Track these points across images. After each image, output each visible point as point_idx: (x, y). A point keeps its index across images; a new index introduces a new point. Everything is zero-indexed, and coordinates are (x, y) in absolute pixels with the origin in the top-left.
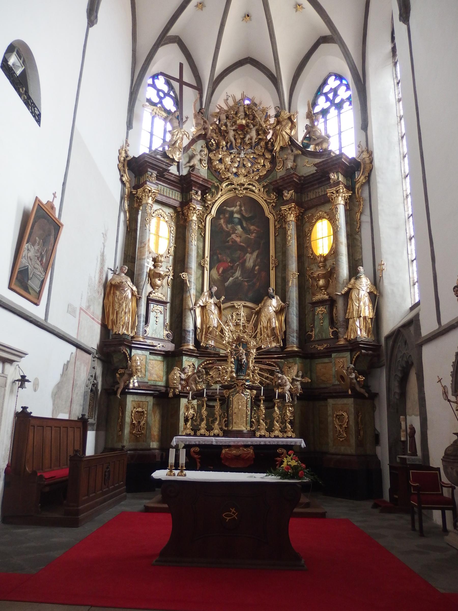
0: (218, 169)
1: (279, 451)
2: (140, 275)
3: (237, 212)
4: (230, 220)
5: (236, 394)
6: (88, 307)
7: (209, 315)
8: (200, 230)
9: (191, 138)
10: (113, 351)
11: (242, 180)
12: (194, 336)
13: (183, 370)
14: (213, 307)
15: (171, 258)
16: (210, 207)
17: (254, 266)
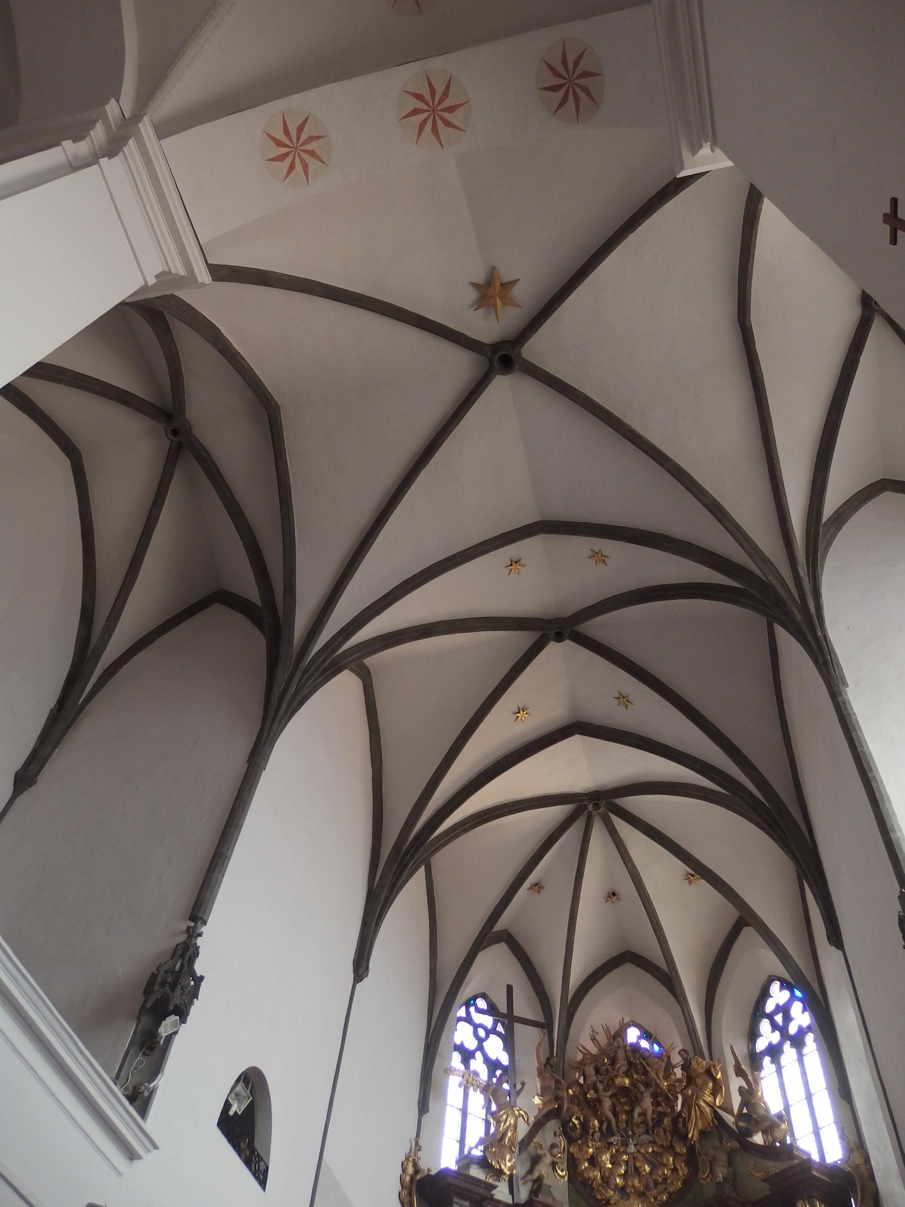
0: (589, 1178)
9: (532, 1120)
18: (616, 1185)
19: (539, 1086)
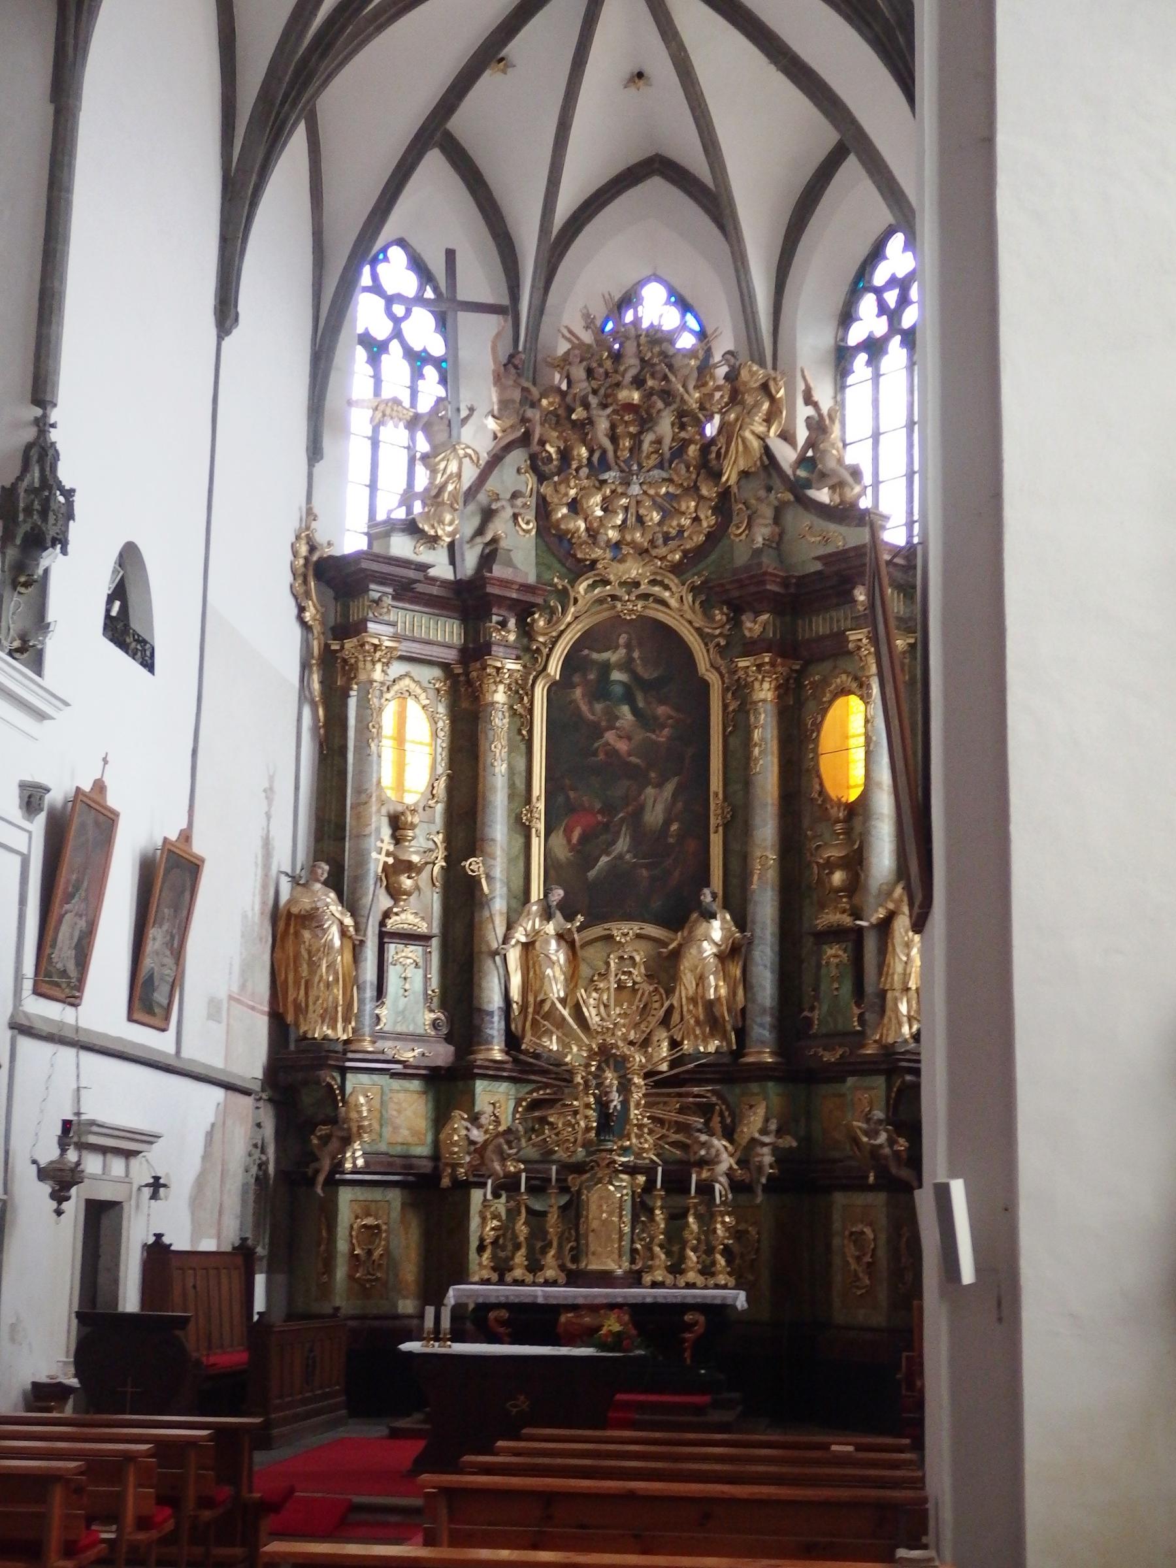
0: (568, 531)
1: (688, 1317)
2: (359, 879)
4: (601, 690)
5: (596, 1184)
6: (243, 987)
7: (543, 968)
8: (517, 719)
10: (300, 1083)
11: (633, 569)
12: (503, 1023)
13: (475, 1119)
14: (553, 944)
15: (440, 808)
16: (545, 651)
17: (667, 823)
18: (609, 540)
19: (495, 399)
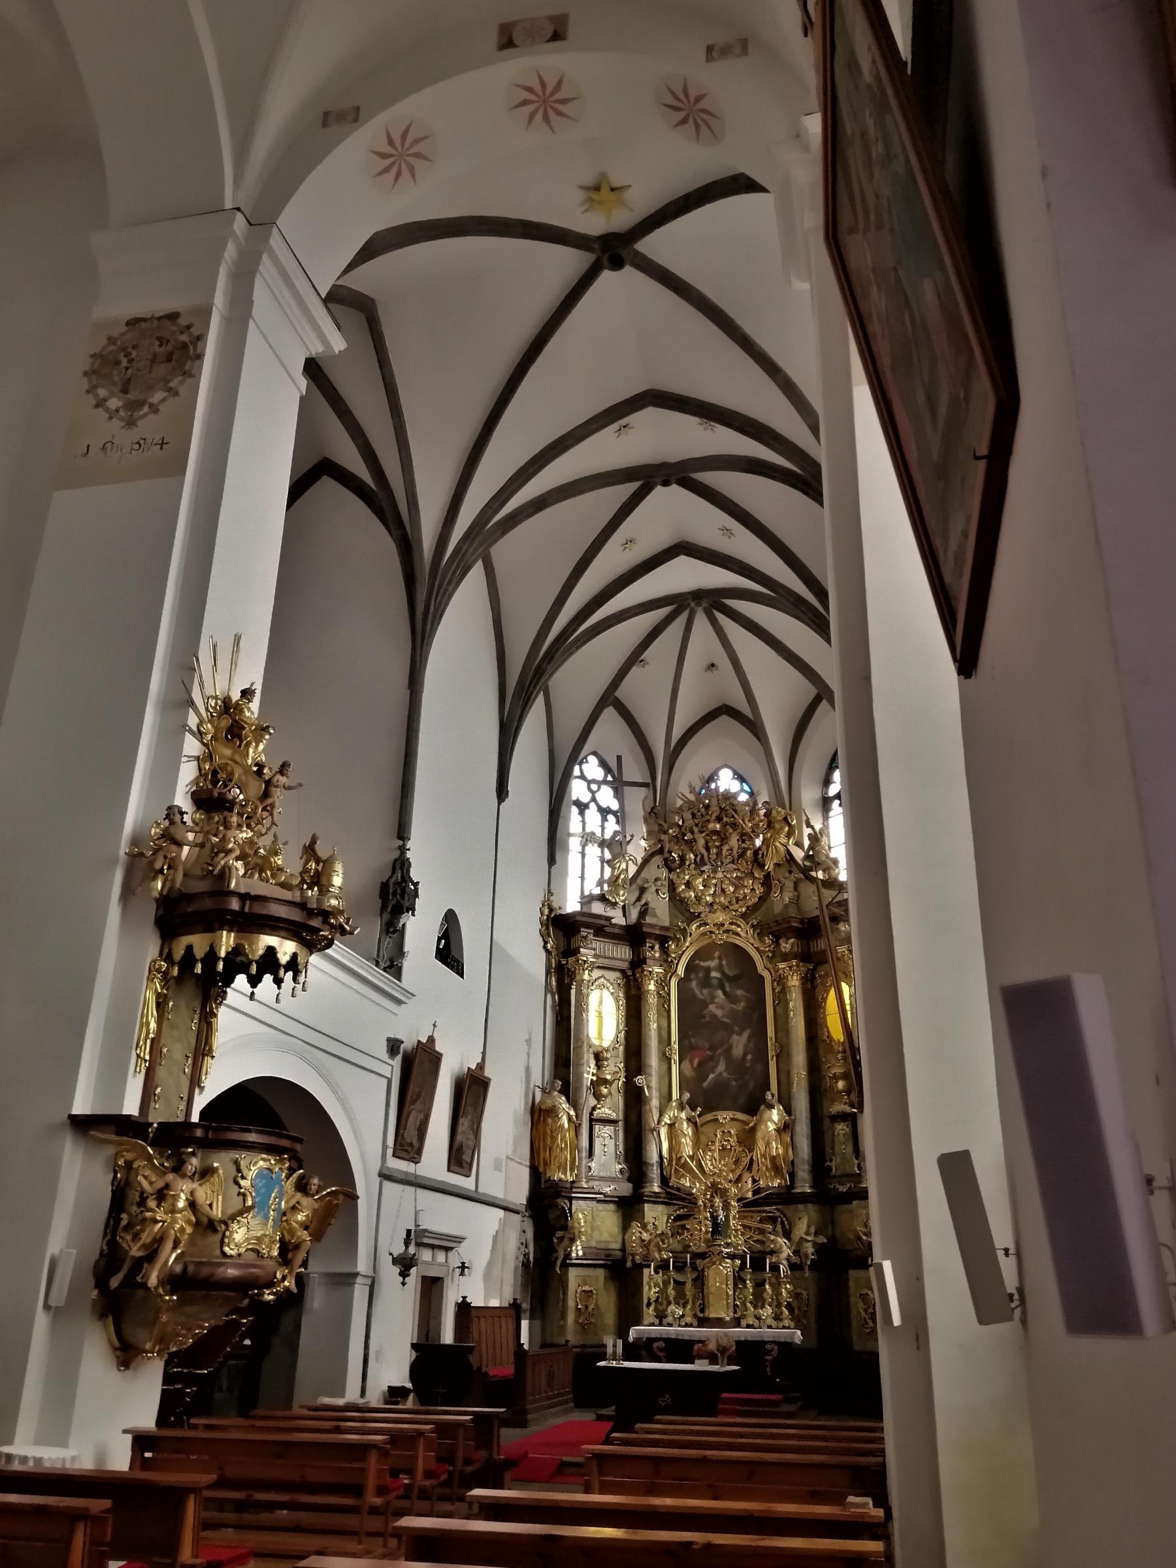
1: (768, 1347)
2: (578, 1089)
3: (715, 969)
4: (706, 982)
6: (515, 1151)
9: (640, 861)
10: (547, 1206)
11: (720, 917)
13: (644, 1226)
14: (685, 1125)
15: (621, 1048)
17: (745, 1055)
